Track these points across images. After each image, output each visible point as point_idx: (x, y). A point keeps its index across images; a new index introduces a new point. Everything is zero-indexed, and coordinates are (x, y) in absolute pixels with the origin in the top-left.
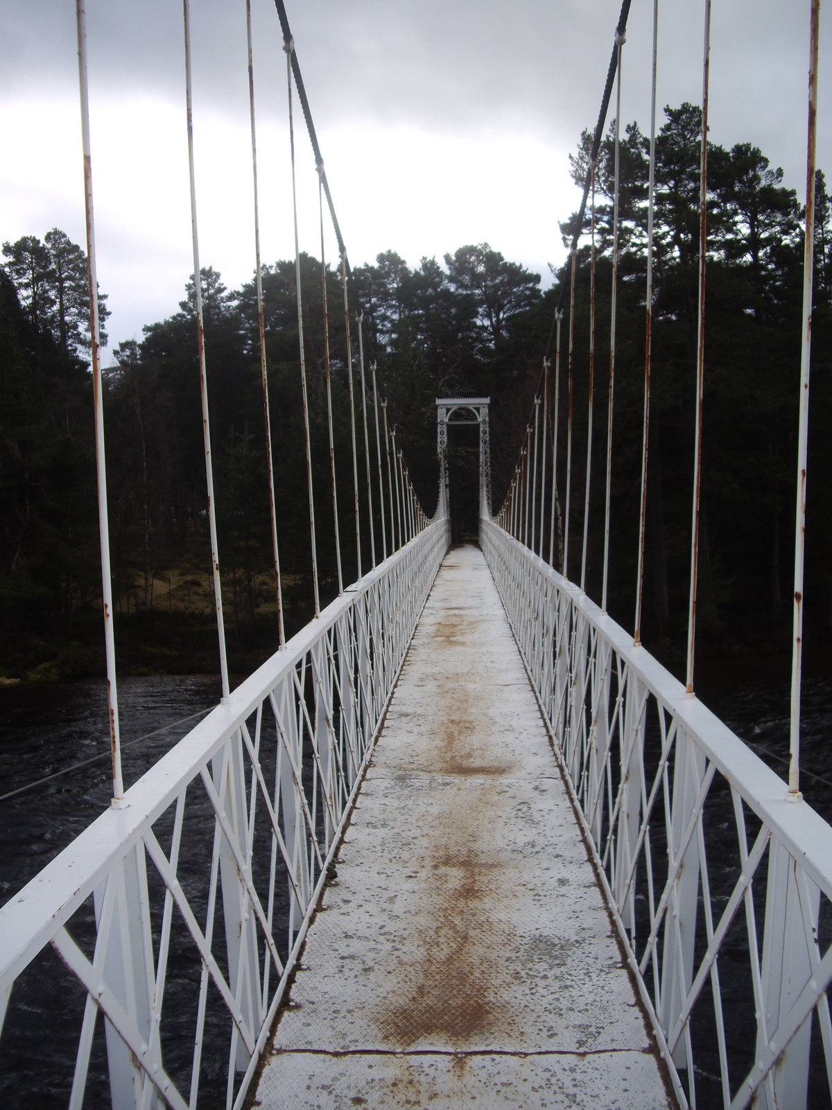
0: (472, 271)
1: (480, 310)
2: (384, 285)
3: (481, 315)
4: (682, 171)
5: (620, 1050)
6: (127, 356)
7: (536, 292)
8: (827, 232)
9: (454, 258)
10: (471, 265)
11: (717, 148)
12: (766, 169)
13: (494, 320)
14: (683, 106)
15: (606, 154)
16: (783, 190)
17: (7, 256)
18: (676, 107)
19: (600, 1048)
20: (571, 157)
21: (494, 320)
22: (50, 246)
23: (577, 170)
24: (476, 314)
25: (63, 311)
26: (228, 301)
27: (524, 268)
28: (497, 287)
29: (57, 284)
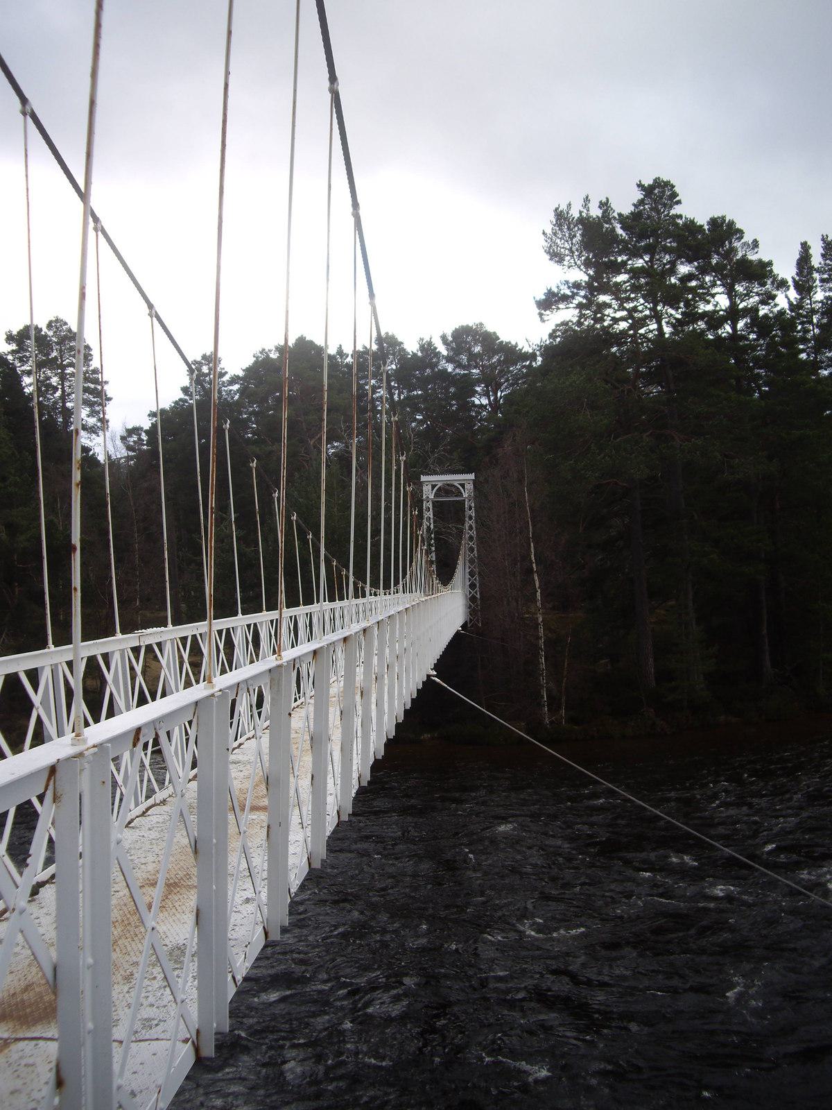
0: (469, 351)
3: (479, 394)
5: (162, 1039)
6: (134, 442)
9: (450, 339)
12: (743, 241)
13: (492, 398)
14: (655, 180)
15: (579, 229)
16: (760, 261)
17: (9, 344)
18: (648, 182)
19: (141, 1038)
20: (544, 233)
21: (492, 398)
22: (52, 334)
23: (551, 246)
24: (474, 393)
25: (64, 398)
26: (228, 385)
27: (520, 347)
29: (59, 371)
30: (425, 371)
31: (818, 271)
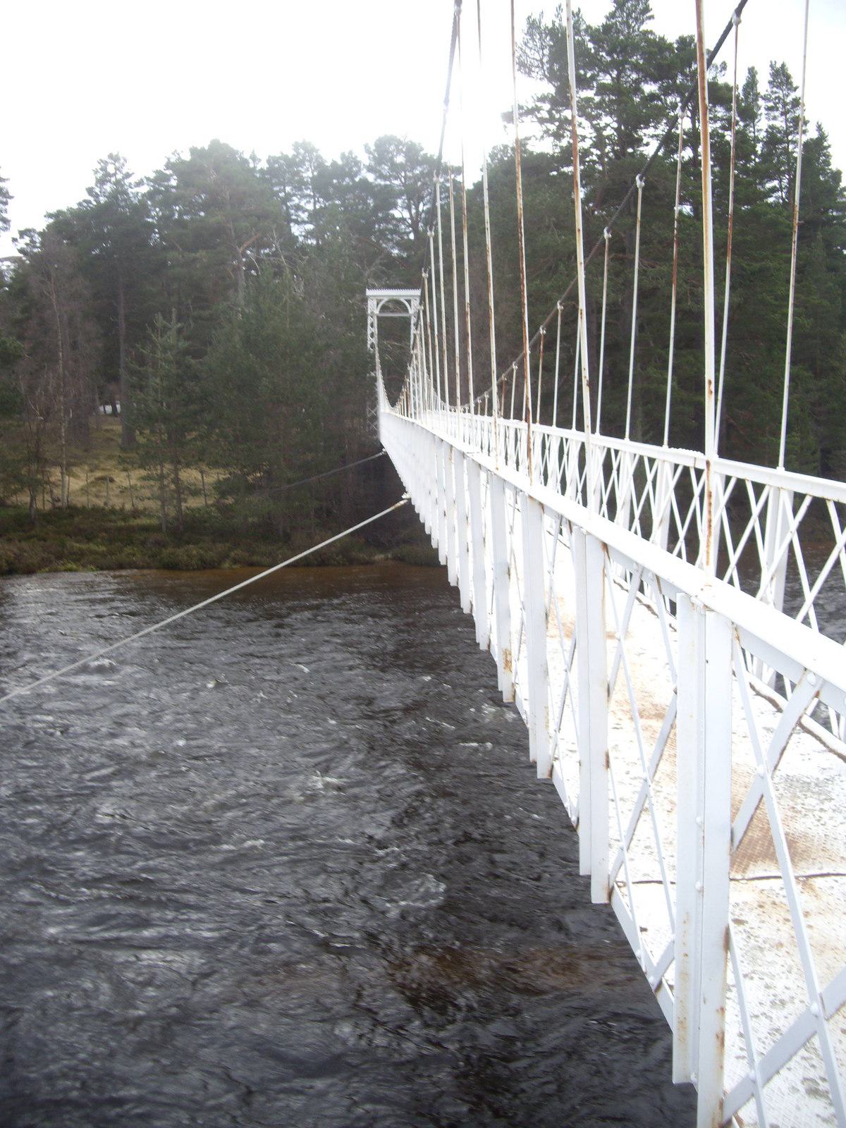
1: (399, 201)
2: (298, 173)
4: (625, 62)
7: (458, 187)
8: (758, 131)
10: (390, 155)
11: (660, 39)
21: (413, 211)
24: (395, 206)
28: (417, 178)
30: (343, 180)
31: (765, 98)
